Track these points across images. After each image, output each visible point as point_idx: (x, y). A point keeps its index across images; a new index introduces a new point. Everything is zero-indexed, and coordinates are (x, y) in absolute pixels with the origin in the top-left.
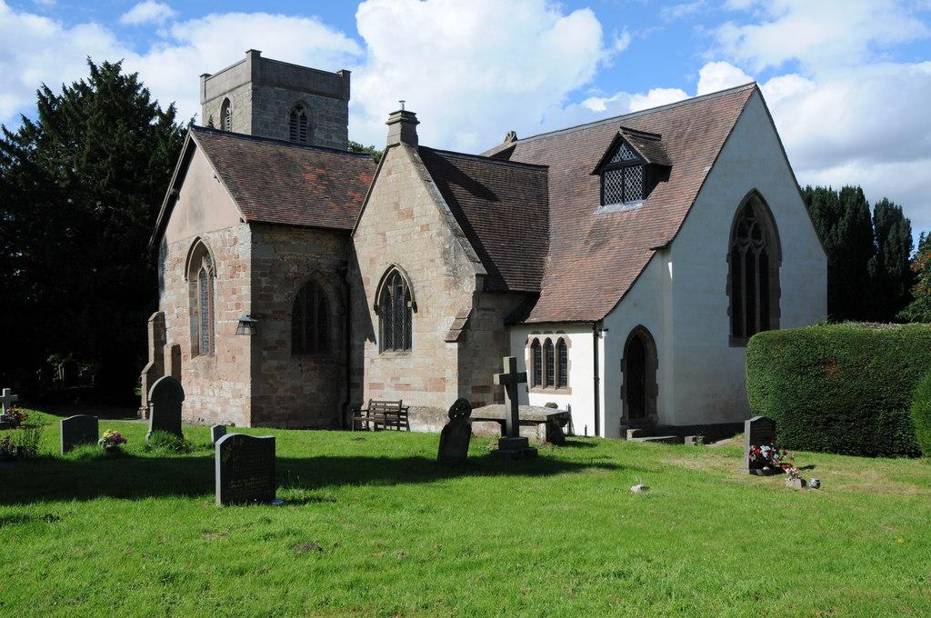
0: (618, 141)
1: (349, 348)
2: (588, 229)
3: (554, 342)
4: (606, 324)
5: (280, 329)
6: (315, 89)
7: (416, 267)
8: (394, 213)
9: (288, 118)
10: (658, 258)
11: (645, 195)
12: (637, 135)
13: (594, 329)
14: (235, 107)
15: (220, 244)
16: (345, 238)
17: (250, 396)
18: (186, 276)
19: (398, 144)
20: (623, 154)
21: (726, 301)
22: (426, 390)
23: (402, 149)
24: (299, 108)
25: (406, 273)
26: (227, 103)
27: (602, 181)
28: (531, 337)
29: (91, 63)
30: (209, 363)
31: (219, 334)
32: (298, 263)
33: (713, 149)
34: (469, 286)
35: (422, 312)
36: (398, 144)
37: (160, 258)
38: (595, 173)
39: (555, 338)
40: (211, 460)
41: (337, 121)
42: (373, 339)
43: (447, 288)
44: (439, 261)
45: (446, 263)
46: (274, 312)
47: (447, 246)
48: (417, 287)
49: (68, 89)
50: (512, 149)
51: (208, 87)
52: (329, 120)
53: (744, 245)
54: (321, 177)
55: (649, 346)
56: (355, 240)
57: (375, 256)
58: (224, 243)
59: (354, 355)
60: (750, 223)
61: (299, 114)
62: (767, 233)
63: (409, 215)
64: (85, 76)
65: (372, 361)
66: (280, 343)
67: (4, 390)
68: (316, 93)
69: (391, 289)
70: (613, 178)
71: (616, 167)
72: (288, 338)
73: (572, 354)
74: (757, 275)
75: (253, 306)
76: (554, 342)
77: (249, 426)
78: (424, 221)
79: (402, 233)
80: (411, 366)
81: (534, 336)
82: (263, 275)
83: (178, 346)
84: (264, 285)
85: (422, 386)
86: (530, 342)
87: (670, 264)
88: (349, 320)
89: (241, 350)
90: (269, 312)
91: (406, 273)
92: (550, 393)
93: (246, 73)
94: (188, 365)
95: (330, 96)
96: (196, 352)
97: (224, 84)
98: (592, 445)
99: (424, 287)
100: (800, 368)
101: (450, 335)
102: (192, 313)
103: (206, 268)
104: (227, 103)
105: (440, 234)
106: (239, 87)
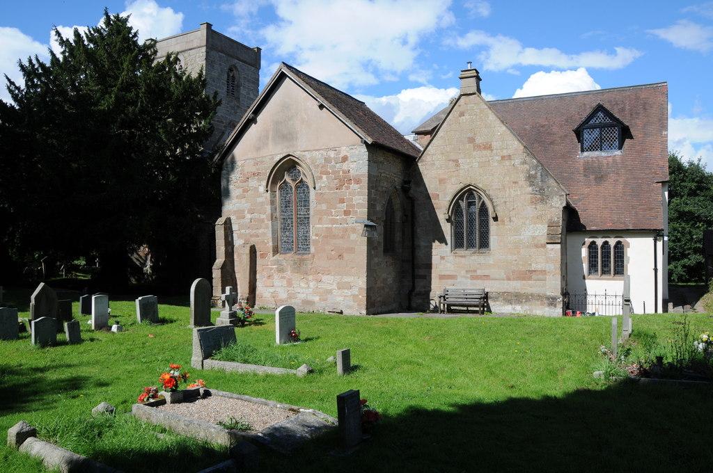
1: (413, 249)
9: (226, 76)
17: (364, 286)
18: (267, 187)
19: (474, 94)
22: (509, 279)
28: (588, 240)
30: (302, 261)
31: (317, 235)
36: (474, 94)
37: (224, 172)
39: (612, 242)
41: (253, 83)
42: (442, 240)
47: (533, 172)
56: (419, 164)
58: (328, 160)
59: (420, 254)
63: (488, 147)
67: (93, 297)
69: (463, 204)
77: (364, 312)
78: (505, 153)
81: (591, 240)
83: (254, 246)
86: (587, 244)
88: (413, 225)
96: (276, 251)
99: (505, 202)
102: (273, 218)
105: (524, 163)
106: (191, 49)
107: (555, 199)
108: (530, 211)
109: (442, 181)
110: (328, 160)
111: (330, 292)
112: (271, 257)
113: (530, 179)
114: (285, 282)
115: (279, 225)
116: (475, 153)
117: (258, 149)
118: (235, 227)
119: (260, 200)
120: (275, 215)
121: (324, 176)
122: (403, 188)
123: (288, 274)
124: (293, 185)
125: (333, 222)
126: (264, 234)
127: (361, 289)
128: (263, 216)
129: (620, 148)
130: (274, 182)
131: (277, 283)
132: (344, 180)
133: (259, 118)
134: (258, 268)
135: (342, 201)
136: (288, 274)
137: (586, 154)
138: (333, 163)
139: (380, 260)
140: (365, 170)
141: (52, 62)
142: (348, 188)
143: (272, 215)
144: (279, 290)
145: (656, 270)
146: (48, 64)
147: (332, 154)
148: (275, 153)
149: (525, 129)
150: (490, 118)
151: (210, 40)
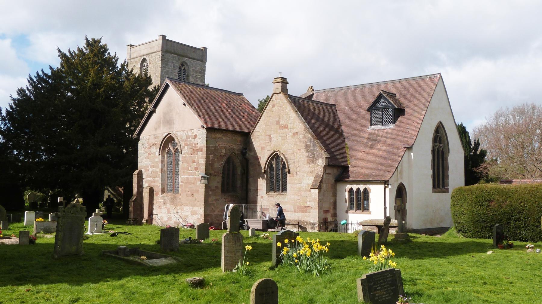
0: (380, 96)
2: (366, 136)
3: (362, 190)
4: (390, 182)
5: (217, 182)
6: (191, 56)
7: (290, 152)
8: (277, 126)
9: (177, 70)
10: (407, 151)
11: (394, 123)
12: (389, 94)
13: (385, 184)
14: (150, 63)
15: (185, 137)
16: (246, 137)
17: (203, 214)
20: (382, 103)
21: (431, 172)
22: (295, 212)
23: (281, 96)
24: (182, 65)
25: (284, 155)
26: (144, 60)
27: (371, 115)
28: (348, 187)
29: (87, 39)
30: (175, 197)
31: (182, 182)
32: (225, 148)
33: (425, 102)
34: (322, 163)
35: (293, 174)
38: (368, 110)
39: (362, 187)
40: (219, 244)
41: (200, 73)
43: (309, 163)
44: (303, 150)
45: (308, 151)
46: (215, 172)
47: (309, 143)
48: (290, 162)
49: (72, 51)
50: (313, 95)
51: (131, 52)
52: (196, 72)
53: (436, 146)
54: (227, 105)
55: (404, 192)
57: (264, 146)
58: (188, 137)
60: (438, 136)
61: (183, 68)
62: (444, 142)
63: (286, 127)
64: (82, 45)
65: (262, 197)
66: (217, 187)
68: (191, 58)
69: (274, 163)
70: (377, 114)
71: (379, 109)
72: (220, 185)
73: (371, 196)
74: (440, 160)
75: (207, 169)
76: (362, 190)
78: (295, 131)
79: (280, 135)
80: (286, 200)
82: (211, 154)
84: (211, 159)
85: (293, 210)
87: (412, 154)
89: (197, 191)
90: (213, 172)
91: (284, 155)
92: (359, 213)
93: (158, 45)
94: (158, 198)
95: (197, 60)
96: (163, 191)
97: (143, 51)
98: (197, 243)
100: (479, 203)
101: (312, 186)
102: (162, 171)
103: (171, 149)
104: (144, 60)
107: (320, 160)
108: (307, 168)
109: (262, 149)
110: (188, 137)
111: (187, 216)
112: (160, 195)
113: (307, 147)
114: (166, 211)
115: (166, 175)
116: (279, 131)
117: (156, 129)
118: (144, 176)
119: (156, 160)
120: (164, 169)
121: (186, 147)
122: (242, 153)
123: (168, 205)
124: (173, 151)
125: (189, 174)
126: (158, 181)
127: (201, 215)
128: (158, 170)
129: (394, 123)
130: (164, 149)
131: (163, 211)
132: (195, 150)
133: (157, 110)
134: (155, 202)
135: (194, 162)
136: (168, 205)
137: (373, 127)
138: (190, 139)
139: (218, 198)
140: (204, 144)
141: (52, 72)
142: (197, 154)
143: (162, 169)
144: (163, 215)
145: (385, 208)
146: (50, 74)
147: (190, 133)
148: (163, 133)
149: (345, 109)
150: (288, 109)
151: (165, 46)
